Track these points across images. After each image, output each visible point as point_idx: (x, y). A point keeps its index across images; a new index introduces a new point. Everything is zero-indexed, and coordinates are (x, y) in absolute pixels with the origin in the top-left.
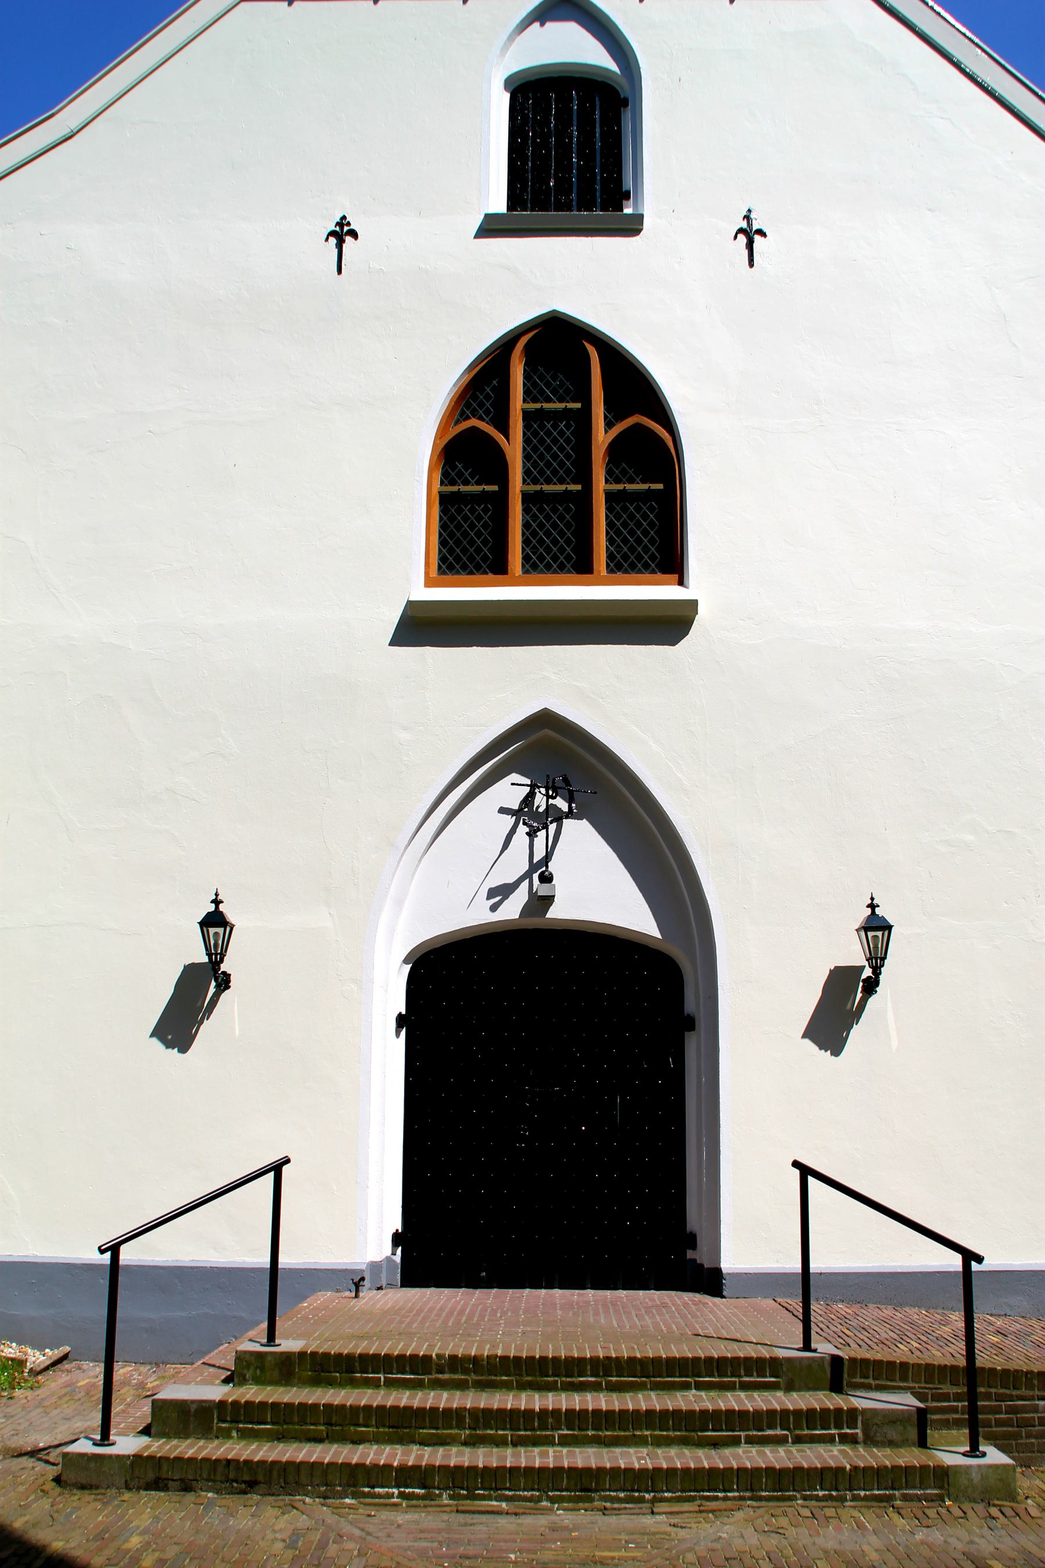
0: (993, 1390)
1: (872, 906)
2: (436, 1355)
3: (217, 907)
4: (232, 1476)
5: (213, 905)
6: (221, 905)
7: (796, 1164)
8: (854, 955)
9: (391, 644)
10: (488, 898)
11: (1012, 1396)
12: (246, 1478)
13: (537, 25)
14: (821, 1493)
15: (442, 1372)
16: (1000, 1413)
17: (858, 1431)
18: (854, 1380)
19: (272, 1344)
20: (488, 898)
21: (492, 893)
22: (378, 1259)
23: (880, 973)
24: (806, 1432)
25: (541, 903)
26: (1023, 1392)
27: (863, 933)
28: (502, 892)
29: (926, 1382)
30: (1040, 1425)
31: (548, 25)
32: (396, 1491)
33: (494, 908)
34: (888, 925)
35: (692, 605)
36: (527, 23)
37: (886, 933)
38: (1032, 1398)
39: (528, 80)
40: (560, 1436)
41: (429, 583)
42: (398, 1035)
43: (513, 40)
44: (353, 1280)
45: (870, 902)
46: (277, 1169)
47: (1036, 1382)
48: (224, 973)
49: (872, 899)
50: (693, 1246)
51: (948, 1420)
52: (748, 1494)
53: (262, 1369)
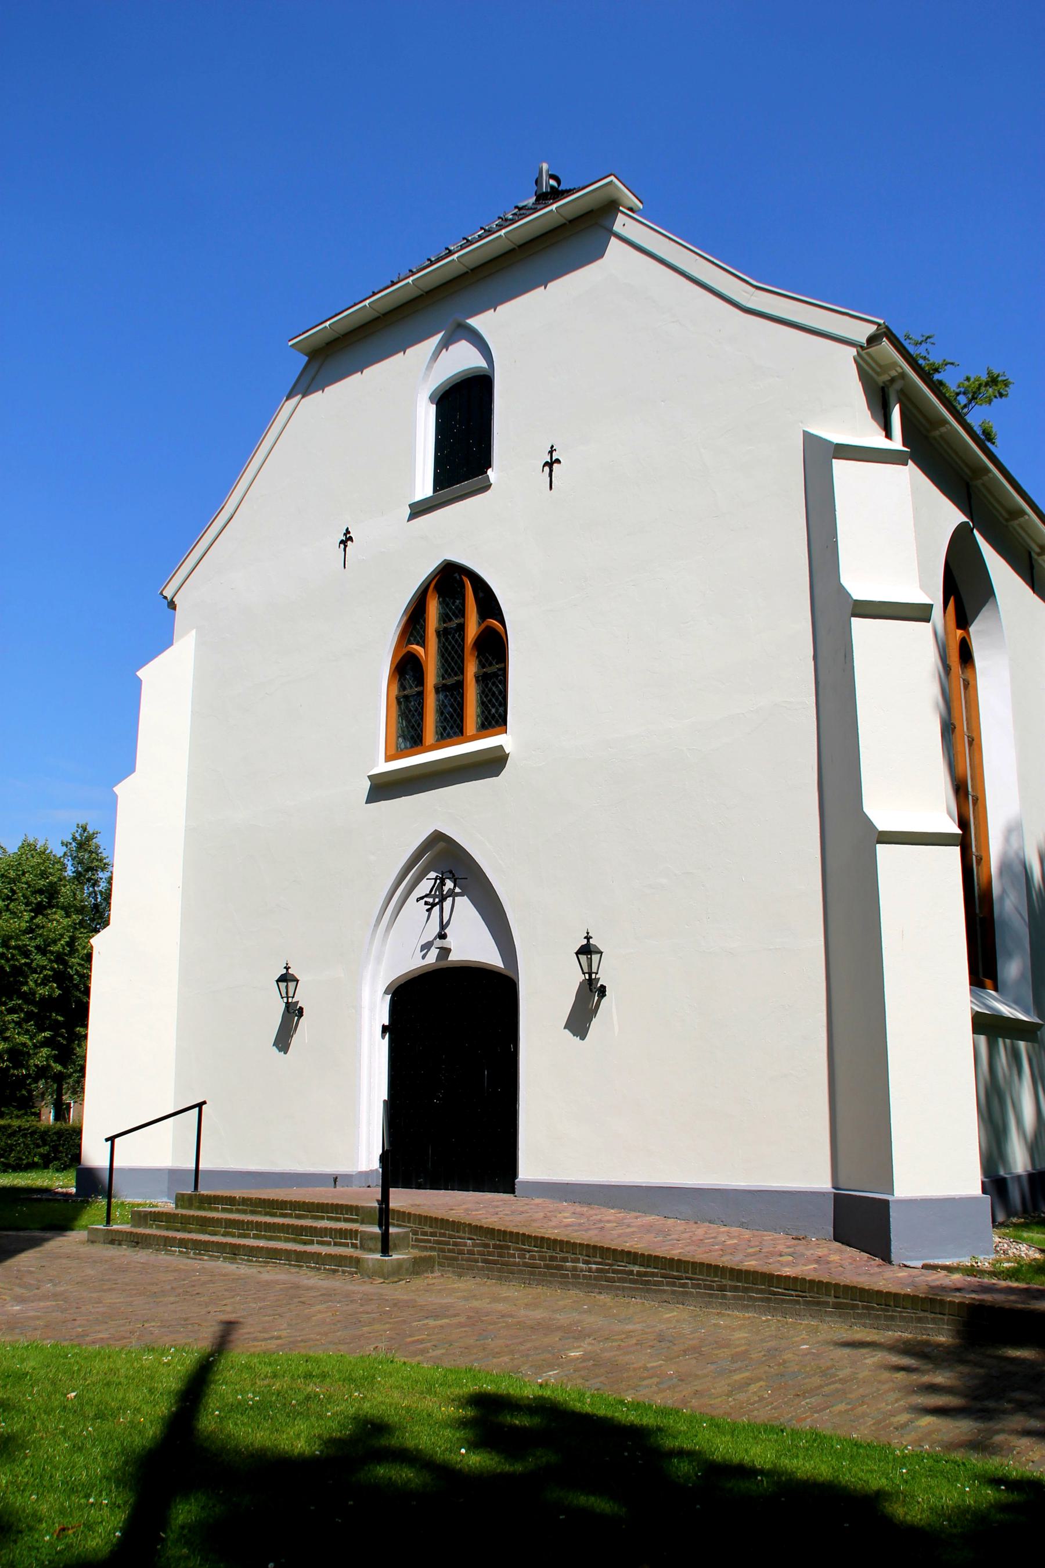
0: (447, 1232)
3: (588, 941)
4: (132, 1239)
5: (285, 970)
6: (591, 940)
9: (366, 803)
10: (421, 951)
11: (455, 1236)
12: (136, 1240)
13: (444, 350)
14: (313, 1265)
15: (239, 1205)
16: (450, 1245)
17: (358, 1242)
20: (421, 951)
21: (423, 948)
24: (338, 1240)
25: (445, 952)
26: (461, 1234)
28: (427, 947)
29: (419, 1225)
30: (468, 1254)
31: (450, 348)
32: (177, 1249)
33: (424, 957)
36: (437, 353)
38: (463, 1238)
39: (444, 390)
40: (253, 1234)
41: (389, 758)
42: (383, 1037)
43: (432, 368)
45: (586, 935)
46: (200, 1105)
47: (467, 1229)
48: (602, 986)
49: (588, 933)
51: (426, 1246)
52: (287, 1262)
53: (183, 1201)
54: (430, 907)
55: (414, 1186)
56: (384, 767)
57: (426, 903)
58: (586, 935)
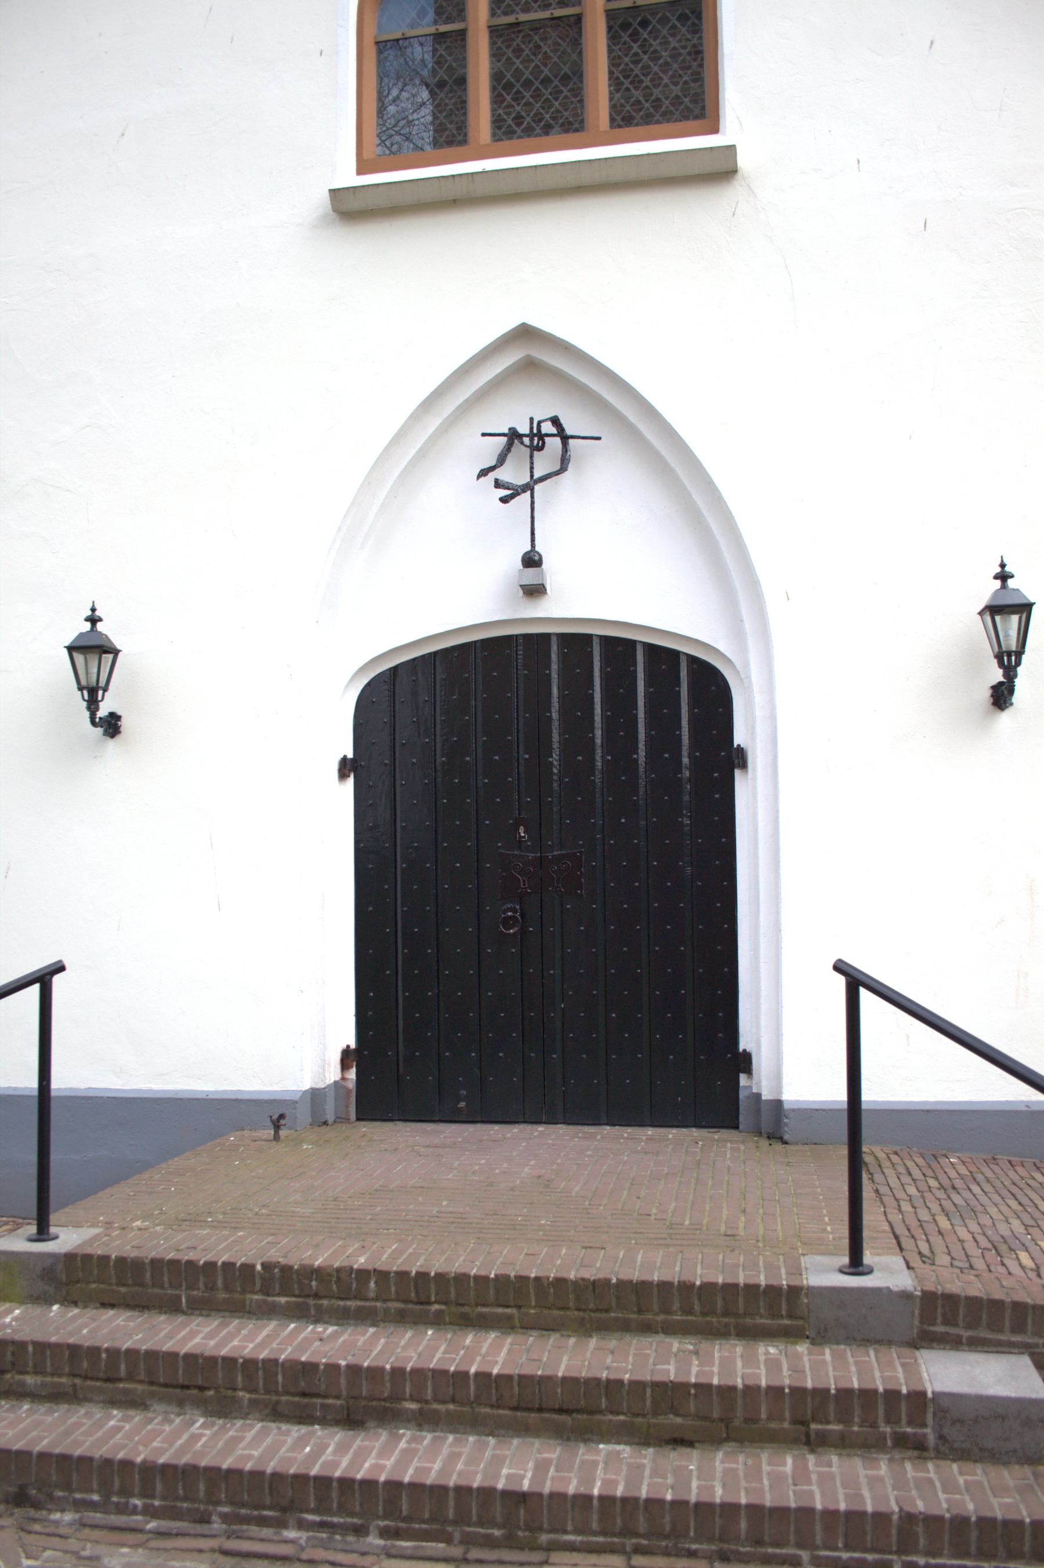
1: (1003, 577)
2: (263, 1265)
5: (998, 583)
6: (99, 625)
7: (840, 967)
8: (997, 675)
17: (928, 1430)
18: (932, 1328)
19: (45, 1237)
22: (321, 1085)
23: (1016, 676)
27: (988, 619)
34: (1025, 601)
35: (731, 149)
37: (1024, 616)
41: (360, 171)
44: (271, 1117)
50: (748, 1070)
54: (508, 492)
55: (602, 1122)
56: (348, 177)
57: (498, 484)
58: (999, 570)
